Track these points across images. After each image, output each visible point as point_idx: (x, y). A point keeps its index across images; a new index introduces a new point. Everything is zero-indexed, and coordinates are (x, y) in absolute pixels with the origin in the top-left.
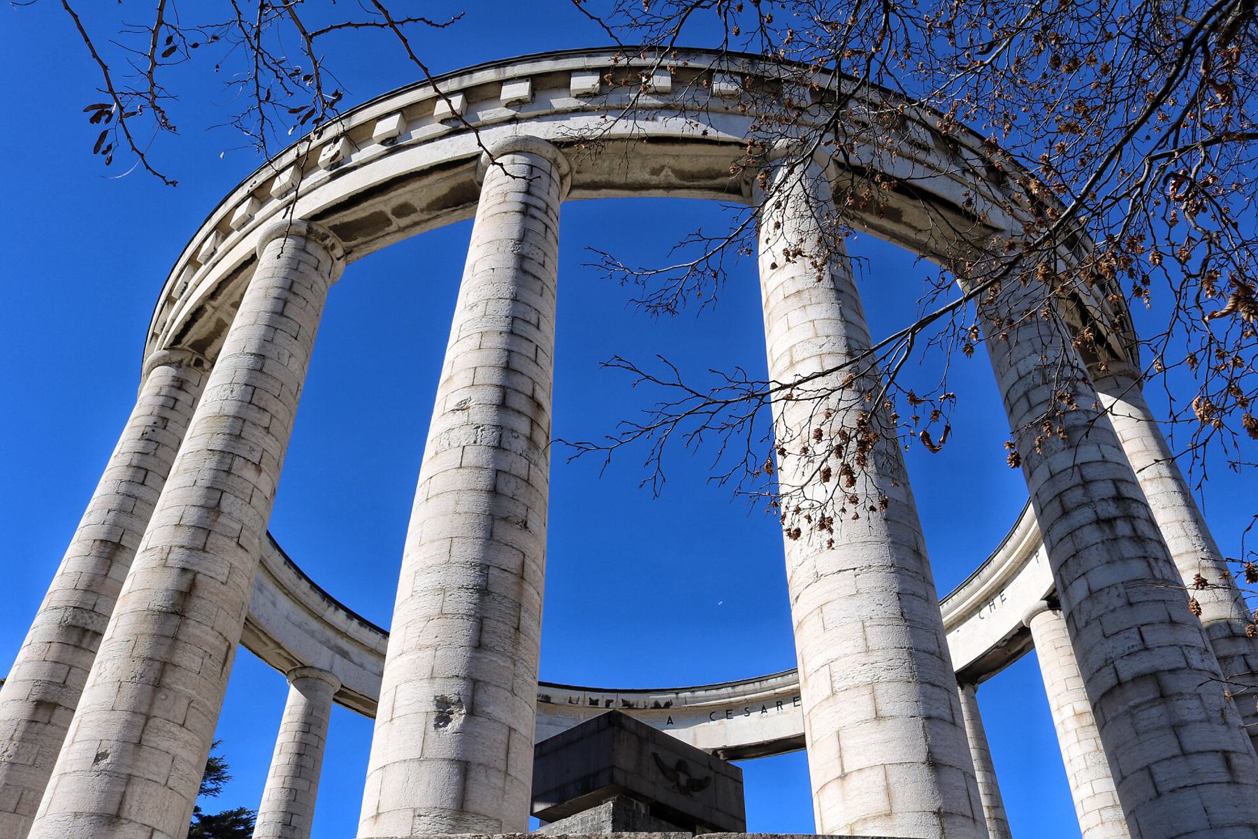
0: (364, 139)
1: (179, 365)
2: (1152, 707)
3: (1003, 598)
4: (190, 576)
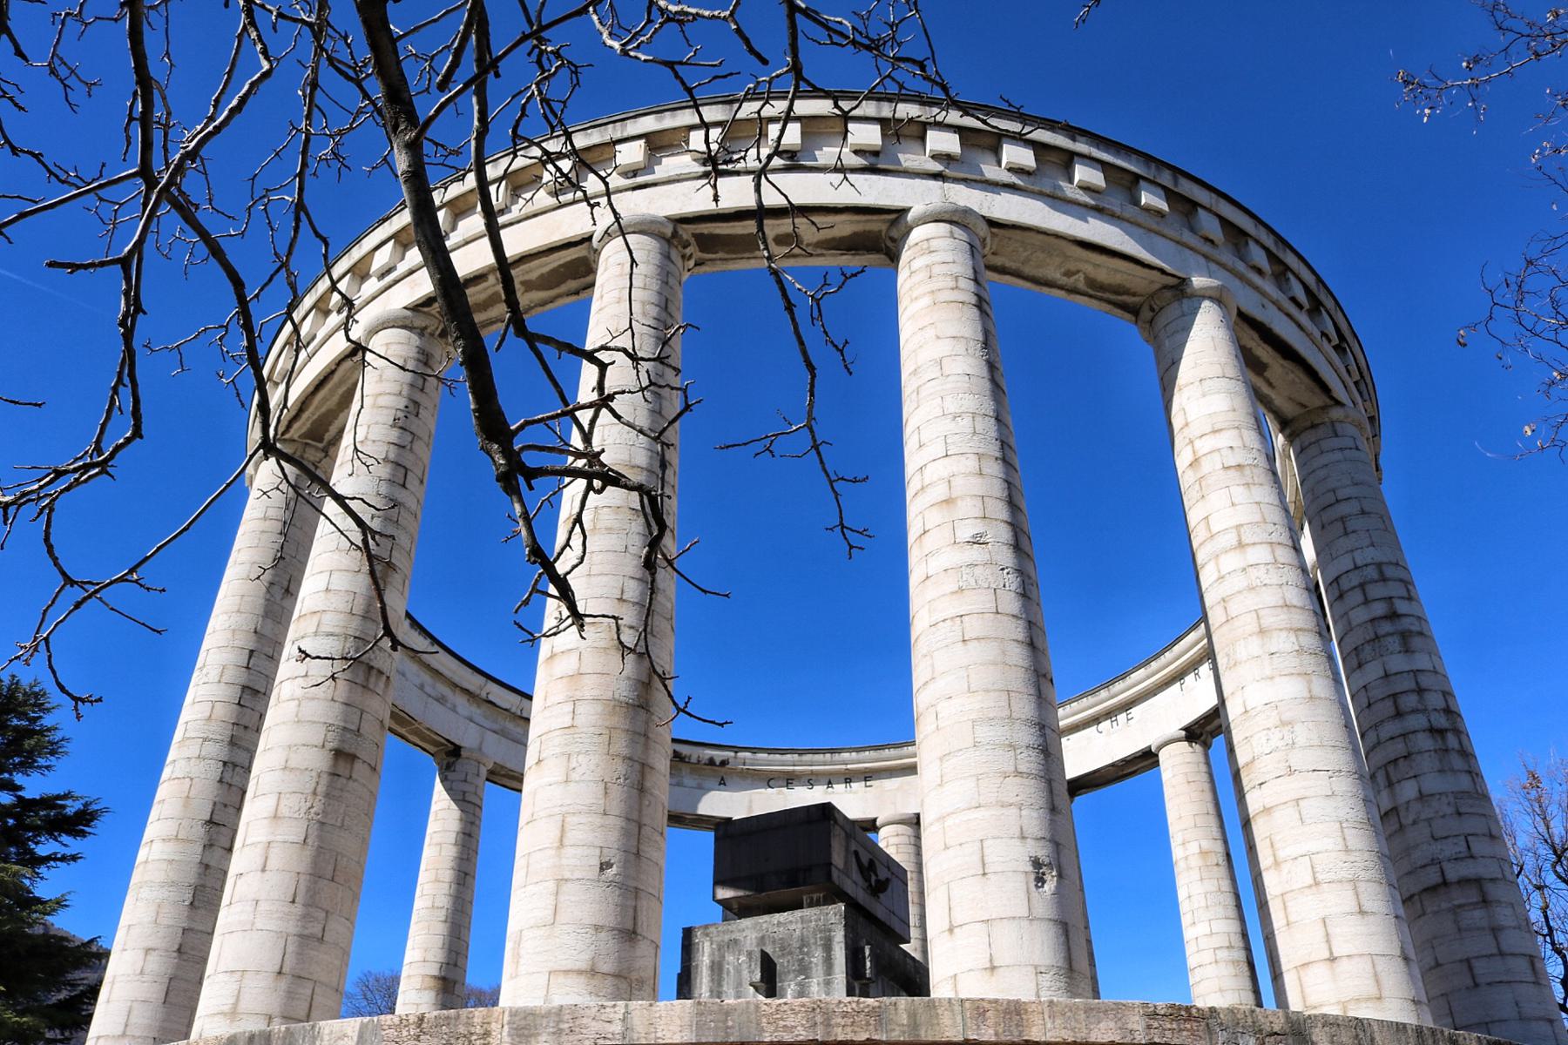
0: (740, 135)
1: (421, 332)
2: (1475, 909)
3: (1130, 717)
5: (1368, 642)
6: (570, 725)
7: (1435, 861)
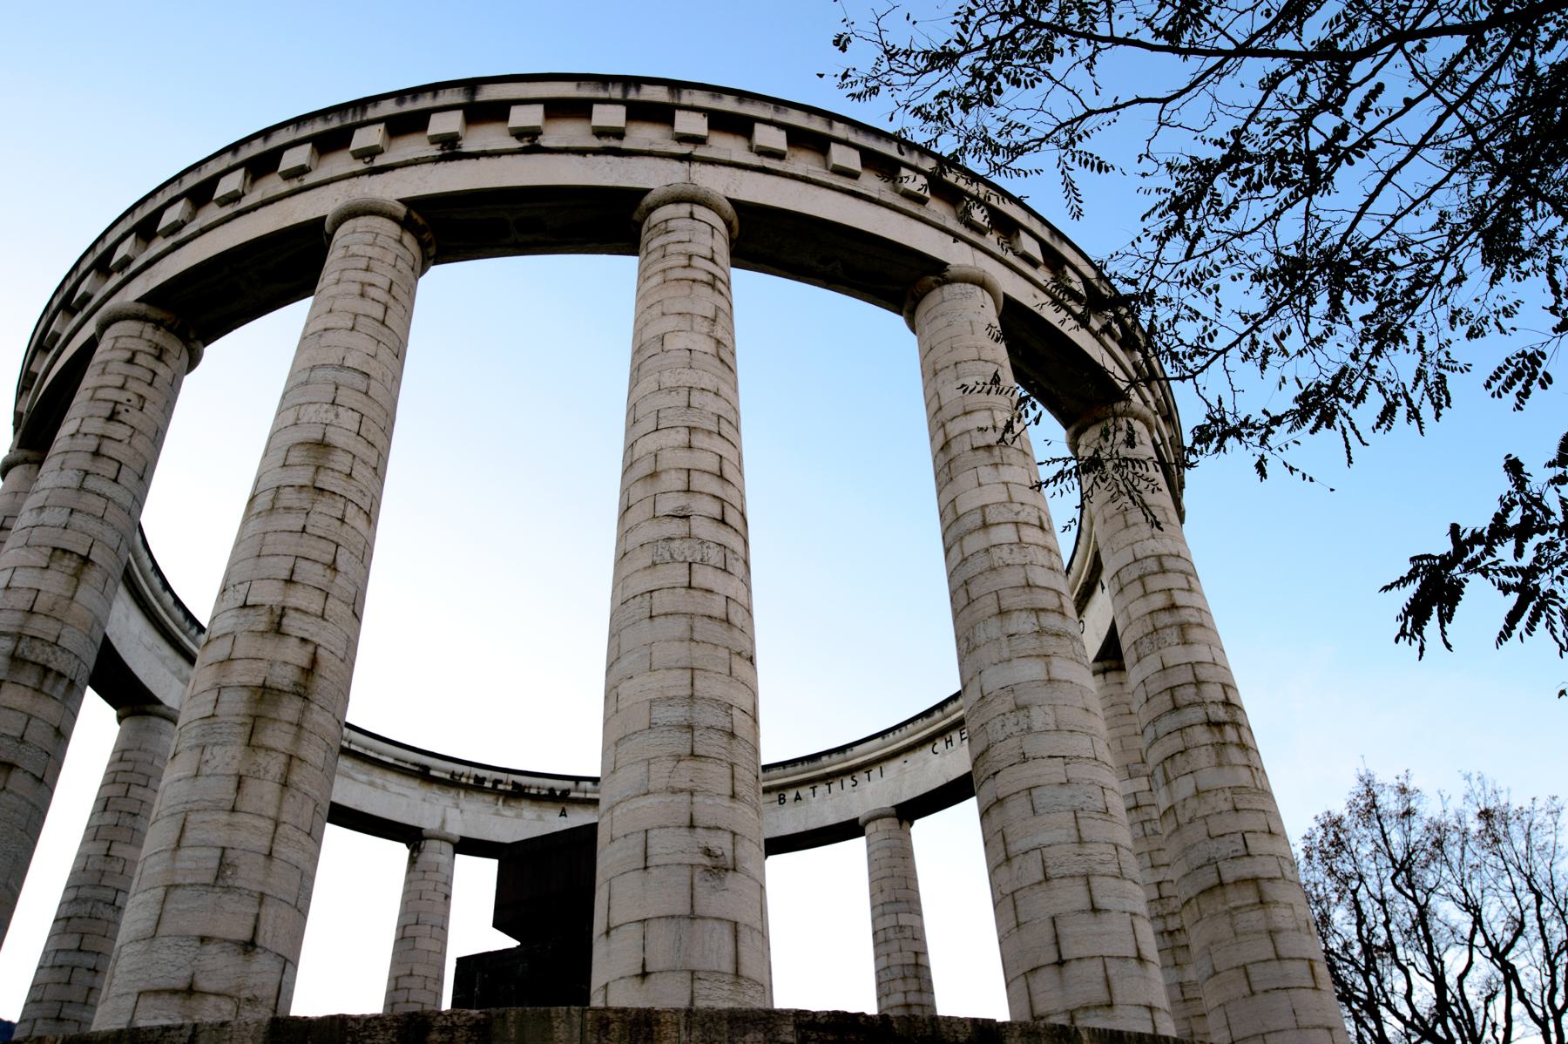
4: (310, 648)
5: (1147, 635)
6: (210, 713)
7: (1211, 862)
